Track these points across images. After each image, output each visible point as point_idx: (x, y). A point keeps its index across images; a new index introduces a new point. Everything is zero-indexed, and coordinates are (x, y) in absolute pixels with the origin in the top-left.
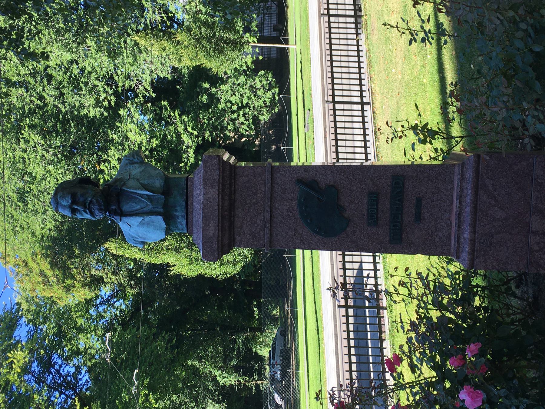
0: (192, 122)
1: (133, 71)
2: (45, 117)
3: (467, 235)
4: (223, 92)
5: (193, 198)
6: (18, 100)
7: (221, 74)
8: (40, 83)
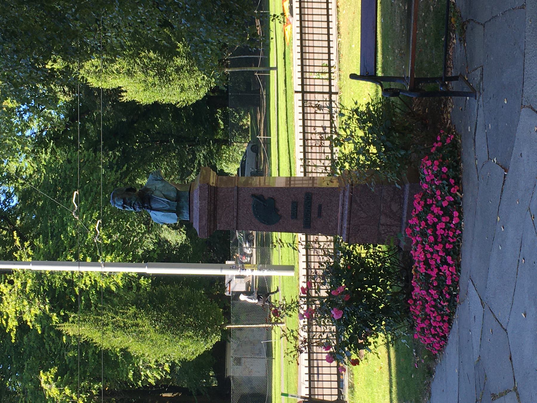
3: (345, 225)
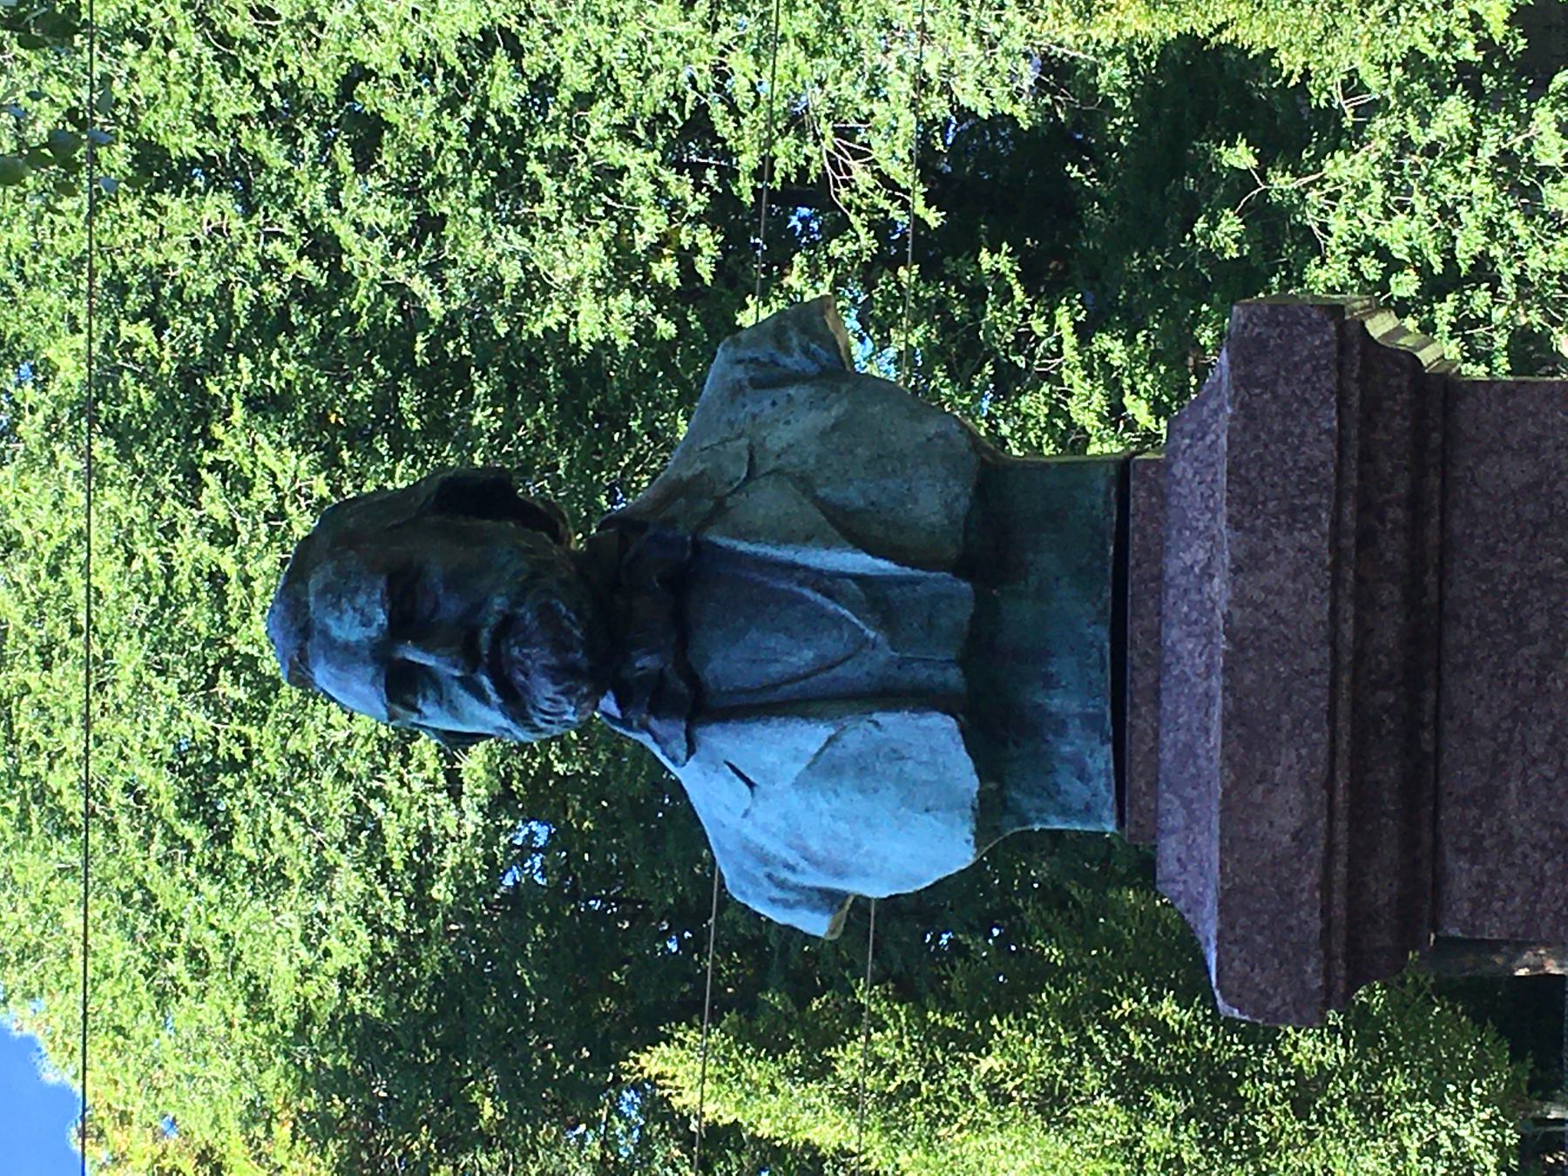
0: (1151, 367)
1: (821, 84)
4: (1335, 196)
5: (1158, 594)
6: (196, 258)
7: (1326, 92)
8: (315, 165)
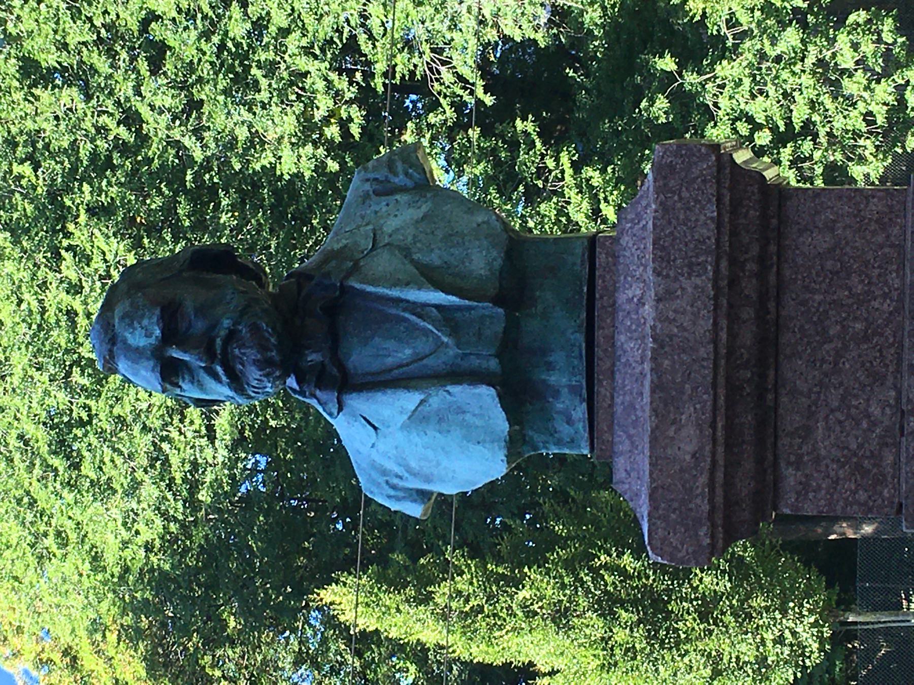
0: (616, 187)
2: (140, 179)
4: (722, 86)
5: (613, 314)
7: (717, 24)
8: (126, 71)
